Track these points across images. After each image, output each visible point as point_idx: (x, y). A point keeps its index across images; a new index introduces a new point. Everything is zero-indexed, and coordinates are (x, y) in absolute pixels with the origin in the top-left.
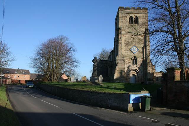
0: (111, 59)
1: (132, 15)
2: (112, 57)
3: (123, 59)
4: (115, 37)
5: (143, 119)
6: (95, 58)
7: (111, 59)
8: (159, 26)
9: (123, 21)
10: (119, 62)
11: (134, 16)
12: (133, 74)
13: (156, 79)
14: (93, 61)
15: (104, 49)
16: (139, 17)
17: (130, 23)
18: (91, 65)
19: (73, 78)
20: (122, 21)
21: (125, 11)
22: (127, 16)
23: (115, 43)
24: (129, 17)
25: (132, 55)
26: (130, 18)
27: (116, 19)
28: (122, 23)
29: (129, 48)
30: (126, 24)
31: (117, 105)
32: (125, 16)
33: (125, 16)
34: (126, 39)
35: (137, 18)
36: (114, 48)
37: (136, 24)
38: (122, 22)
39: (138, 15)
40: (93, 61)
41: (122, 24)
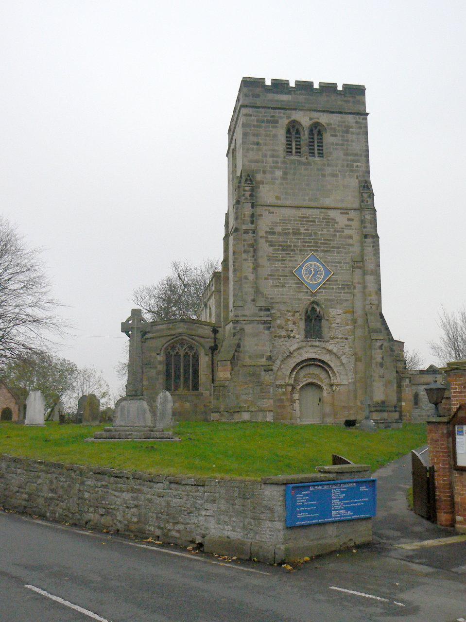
0: (213, 315)
1: (298, 116)
2: (218, 305)
3: (263, 313)
4: (227, 215)
5: (277, 92)
6: (136, 313)
7: (213, 315)
8: (170, 558)
9: (261, 142)
10: (248, 329)
11: (305, 120)
12: (310, 380)
13: (412, 403)
14: (126, 328)
15: (182, 265)
16: (329, 124)
17: (289, 152)
18: (120, 348)
19: (162, 376)
20: (258, 144)
21: (270, 96)
22: (277, 122)
23: (226, 238)
24: (284, 122)
25: (301, 296)
26: (288, 131)
27: (228, 133)
28: (258, 150)
29: (290, 264)
30: (273, 156)
31: (231, 534)
32: (268, 122)
33: (268, 122)
34: (275, 224)
35: (317, 130)
36: (225, 262)
37: (317, 159)
38: (255, 147)
39: (324, 119)
40: (126, 328)
41: (256, 157)
